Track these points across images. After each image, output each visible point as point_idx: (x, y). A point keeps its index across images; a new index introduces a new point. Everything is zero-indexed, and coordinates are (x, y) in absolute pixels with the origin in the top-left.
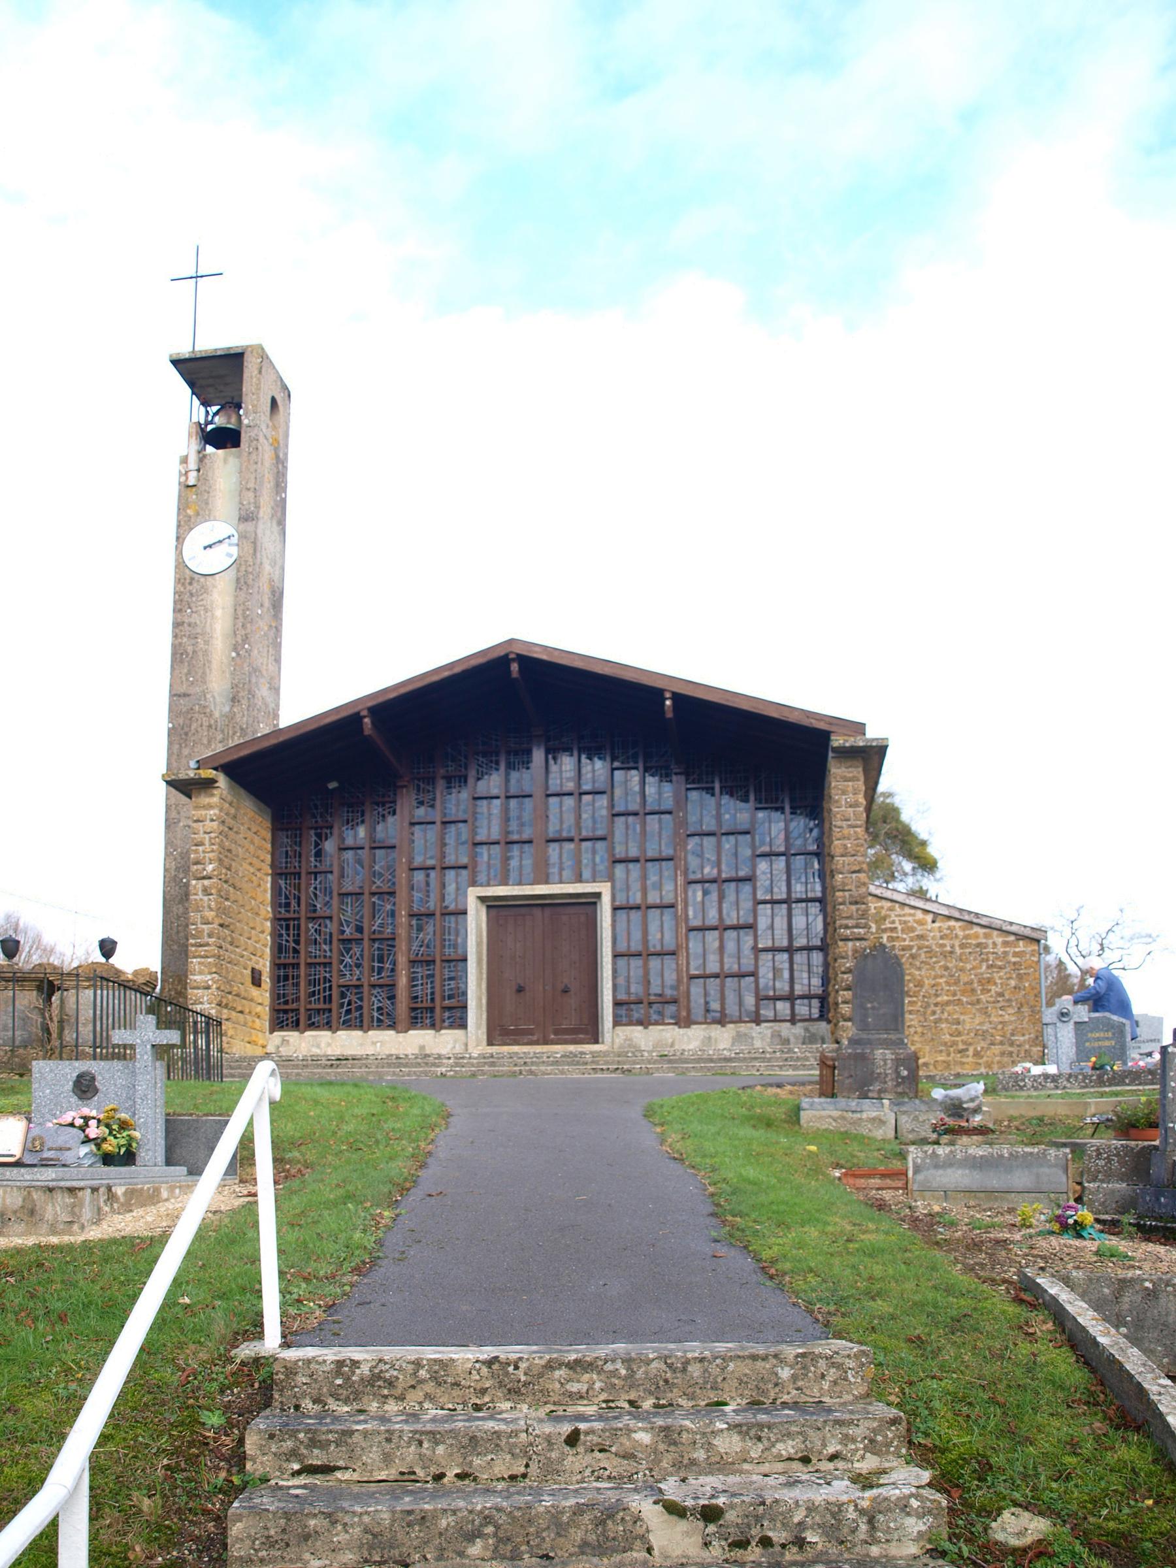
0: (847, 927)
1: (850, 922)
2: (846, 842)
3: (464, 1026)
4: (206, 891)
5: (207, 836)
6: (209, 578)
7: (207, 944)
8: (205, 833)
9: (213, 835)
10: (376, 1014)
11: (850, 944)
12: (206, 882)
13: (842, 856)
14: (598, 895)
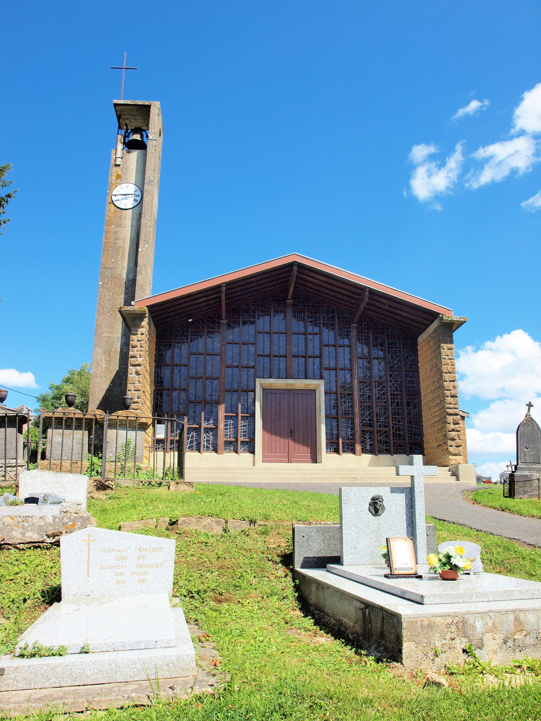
0: (450, 408)
1: (451, 406)
2: (447, 366)
3: (253, 452)
4: (137, 373)
5: (139, 343)
6: (124, 211)
7: (137, 402)
8: (138, 341)
9: (142, 342)
10: (206, 444)
11: (452, 417)
12: (138, 368)
13: (446, 373)
14: (313, 392)
